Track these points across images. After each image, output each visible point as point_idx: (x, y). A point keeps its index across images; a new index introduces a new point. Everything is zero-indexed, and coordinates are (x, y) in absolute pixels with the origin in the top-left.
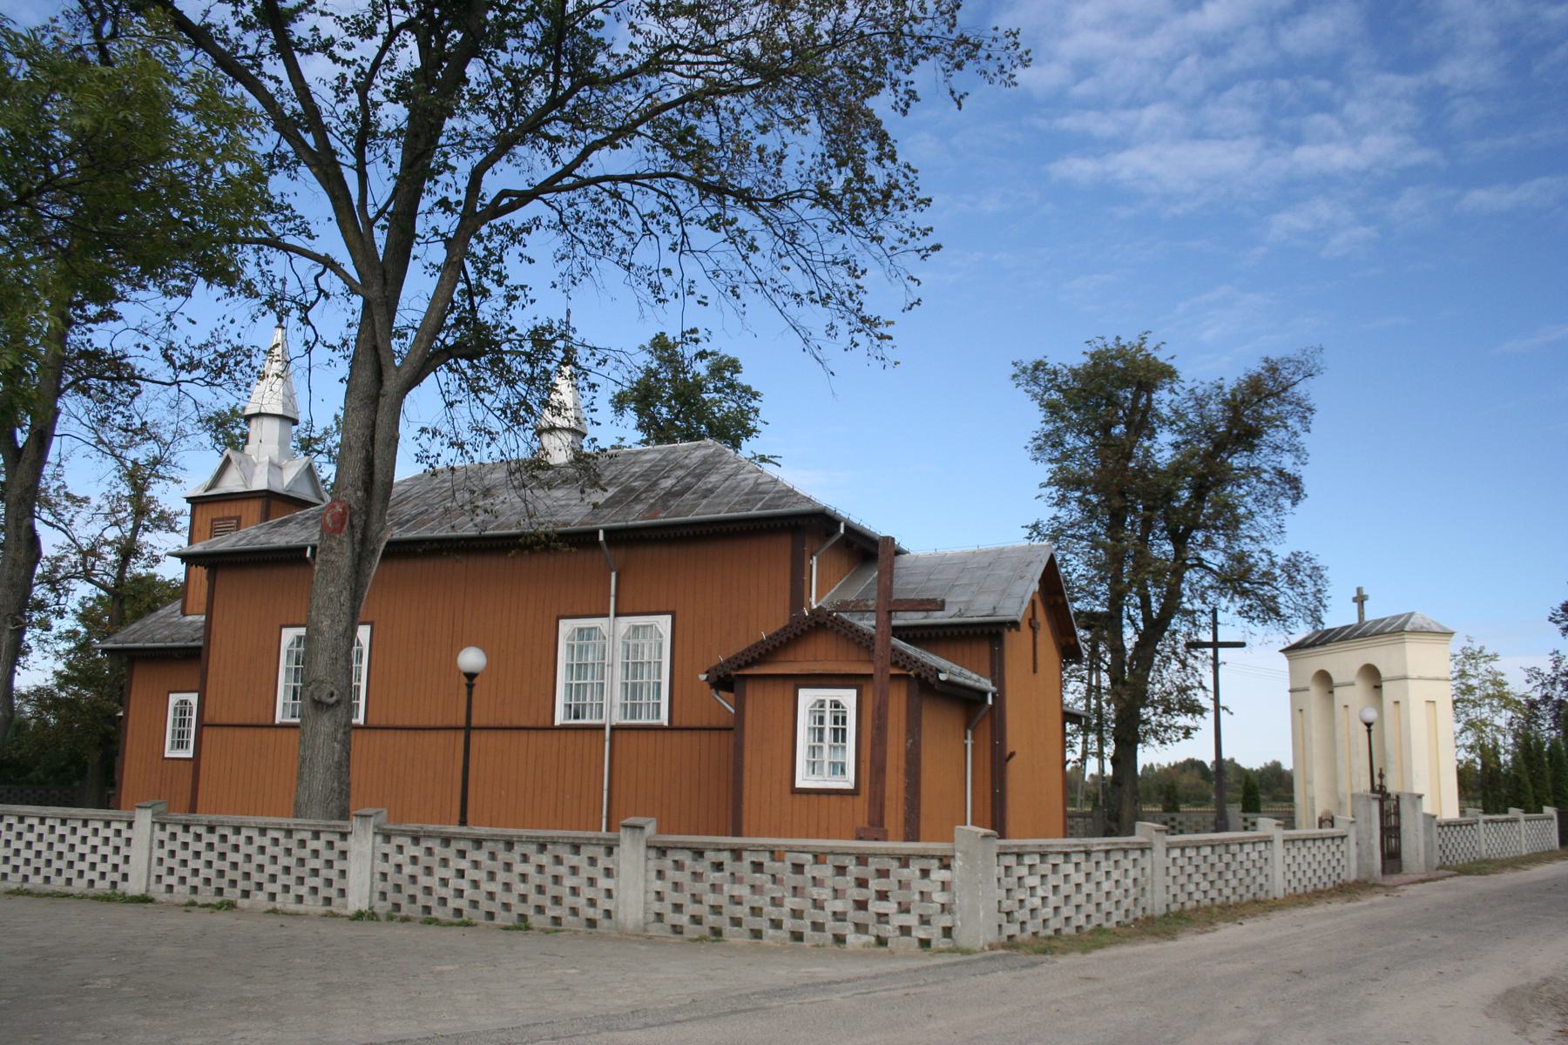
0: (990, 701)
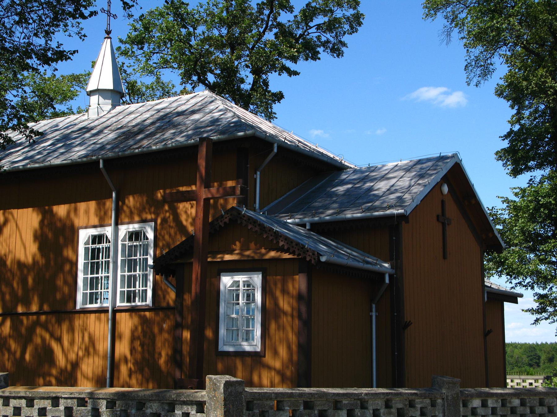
0: (387, 281)
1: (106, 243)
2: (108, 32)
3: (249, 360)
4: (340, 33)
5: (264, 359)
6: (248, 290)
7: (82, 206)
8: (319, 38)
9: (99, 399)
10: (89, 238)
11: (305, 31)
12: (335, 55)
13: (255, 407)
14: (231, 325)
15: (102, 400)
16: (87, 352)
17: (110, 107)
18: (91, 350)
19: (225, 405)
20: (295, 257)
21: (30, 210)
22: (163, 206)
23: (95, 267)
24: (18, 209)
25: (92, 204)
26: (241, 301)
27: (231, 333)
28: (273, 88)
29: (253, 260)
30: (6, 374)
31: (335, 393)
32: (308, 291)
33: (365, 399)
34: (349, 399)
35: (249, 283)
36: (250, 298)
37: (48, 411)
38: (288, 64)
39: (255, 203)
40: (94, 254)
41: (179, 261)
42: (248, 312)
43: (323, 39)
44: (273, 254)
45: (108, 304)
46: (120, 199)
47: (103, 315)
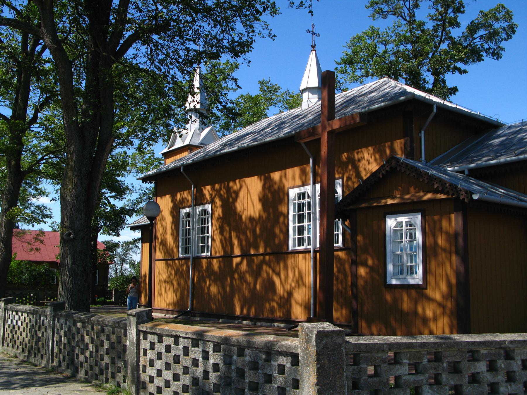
1: (308, 198)
2: (313, 47)
3: (413, 292)
4: (499, 40)
5: (426, 290)
6: (410, 229)
8: (482, 45)
9: (208, 341)
10: (296, 195)
11: (471, 42)
12: (495, 58)
13: (361, 361)
14: (397, 261)
15: (210, 343)
17: (317, 99)
18: (300, 282)
19: (318, 360)
20: (450, 197)
21: (256, 177)
22: (348, 166)
23: (301, 218)
24: (248, 177)
25: (297, 170)
26: (404, 240)
27: (397, 268)
28: (450, 84)
29: (413, 203)
30: (148, 310)
31: (469, 342)
32: (464, 228)
33: (509, 348)
34: (488, 348)
35: (410, 223)
36: (412, 237)
37: (172, 349)
38: (459, 65)
39: (421, 157)
40: (301, 207)
41: (351, 207)
42: (411, 249)
43: (486, 46)
44: (429, 196)
45: (310, 247)
47: (307, 255)
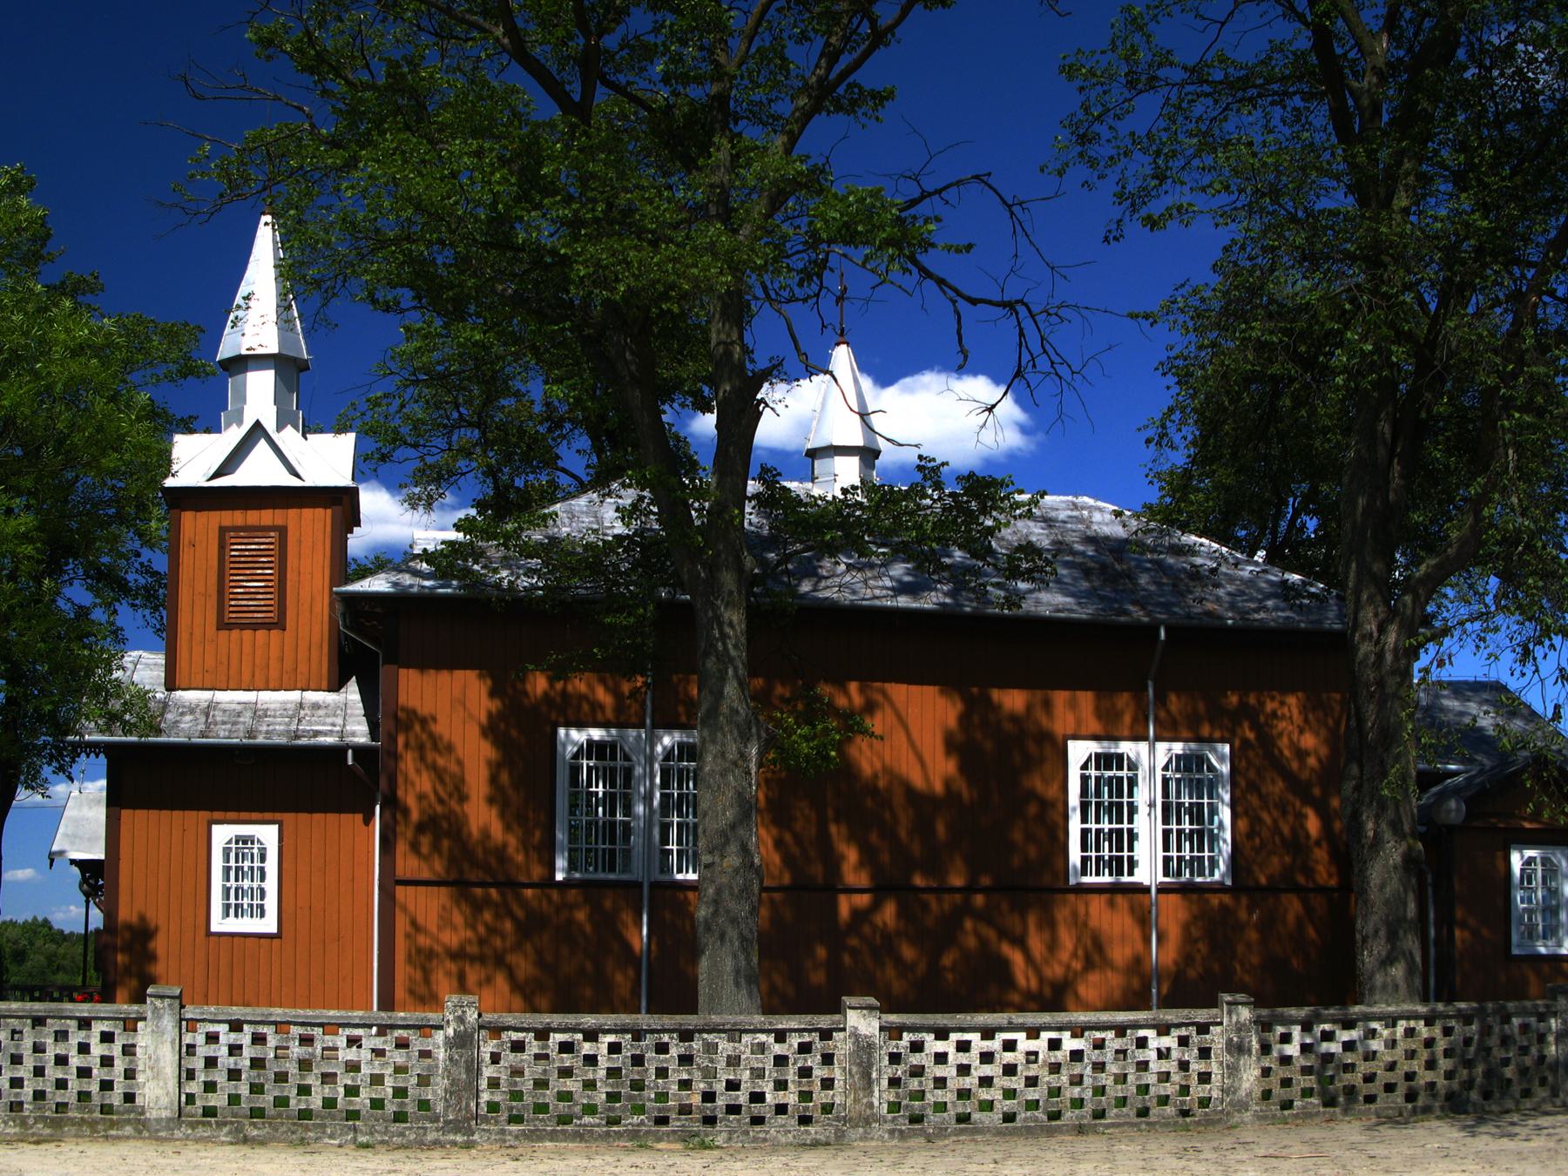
7: (1060, 697)
16: (1089, 965)
18: (1096, 958)
46: (1161, 699)
